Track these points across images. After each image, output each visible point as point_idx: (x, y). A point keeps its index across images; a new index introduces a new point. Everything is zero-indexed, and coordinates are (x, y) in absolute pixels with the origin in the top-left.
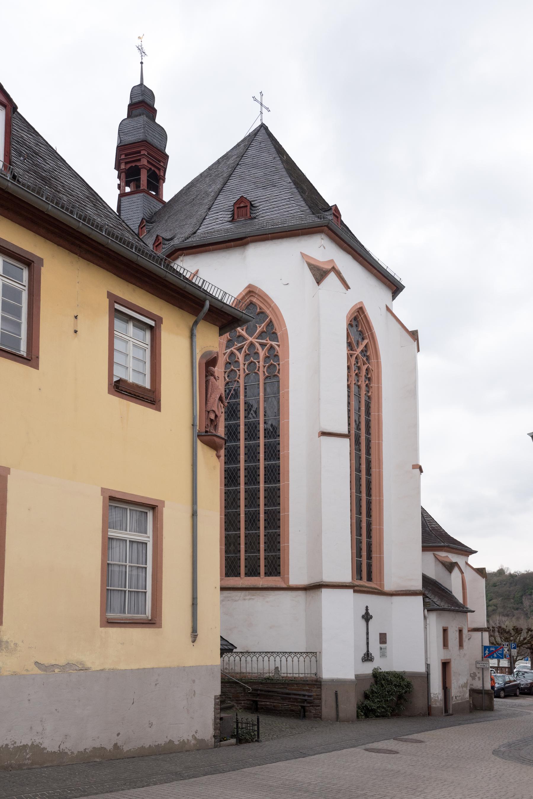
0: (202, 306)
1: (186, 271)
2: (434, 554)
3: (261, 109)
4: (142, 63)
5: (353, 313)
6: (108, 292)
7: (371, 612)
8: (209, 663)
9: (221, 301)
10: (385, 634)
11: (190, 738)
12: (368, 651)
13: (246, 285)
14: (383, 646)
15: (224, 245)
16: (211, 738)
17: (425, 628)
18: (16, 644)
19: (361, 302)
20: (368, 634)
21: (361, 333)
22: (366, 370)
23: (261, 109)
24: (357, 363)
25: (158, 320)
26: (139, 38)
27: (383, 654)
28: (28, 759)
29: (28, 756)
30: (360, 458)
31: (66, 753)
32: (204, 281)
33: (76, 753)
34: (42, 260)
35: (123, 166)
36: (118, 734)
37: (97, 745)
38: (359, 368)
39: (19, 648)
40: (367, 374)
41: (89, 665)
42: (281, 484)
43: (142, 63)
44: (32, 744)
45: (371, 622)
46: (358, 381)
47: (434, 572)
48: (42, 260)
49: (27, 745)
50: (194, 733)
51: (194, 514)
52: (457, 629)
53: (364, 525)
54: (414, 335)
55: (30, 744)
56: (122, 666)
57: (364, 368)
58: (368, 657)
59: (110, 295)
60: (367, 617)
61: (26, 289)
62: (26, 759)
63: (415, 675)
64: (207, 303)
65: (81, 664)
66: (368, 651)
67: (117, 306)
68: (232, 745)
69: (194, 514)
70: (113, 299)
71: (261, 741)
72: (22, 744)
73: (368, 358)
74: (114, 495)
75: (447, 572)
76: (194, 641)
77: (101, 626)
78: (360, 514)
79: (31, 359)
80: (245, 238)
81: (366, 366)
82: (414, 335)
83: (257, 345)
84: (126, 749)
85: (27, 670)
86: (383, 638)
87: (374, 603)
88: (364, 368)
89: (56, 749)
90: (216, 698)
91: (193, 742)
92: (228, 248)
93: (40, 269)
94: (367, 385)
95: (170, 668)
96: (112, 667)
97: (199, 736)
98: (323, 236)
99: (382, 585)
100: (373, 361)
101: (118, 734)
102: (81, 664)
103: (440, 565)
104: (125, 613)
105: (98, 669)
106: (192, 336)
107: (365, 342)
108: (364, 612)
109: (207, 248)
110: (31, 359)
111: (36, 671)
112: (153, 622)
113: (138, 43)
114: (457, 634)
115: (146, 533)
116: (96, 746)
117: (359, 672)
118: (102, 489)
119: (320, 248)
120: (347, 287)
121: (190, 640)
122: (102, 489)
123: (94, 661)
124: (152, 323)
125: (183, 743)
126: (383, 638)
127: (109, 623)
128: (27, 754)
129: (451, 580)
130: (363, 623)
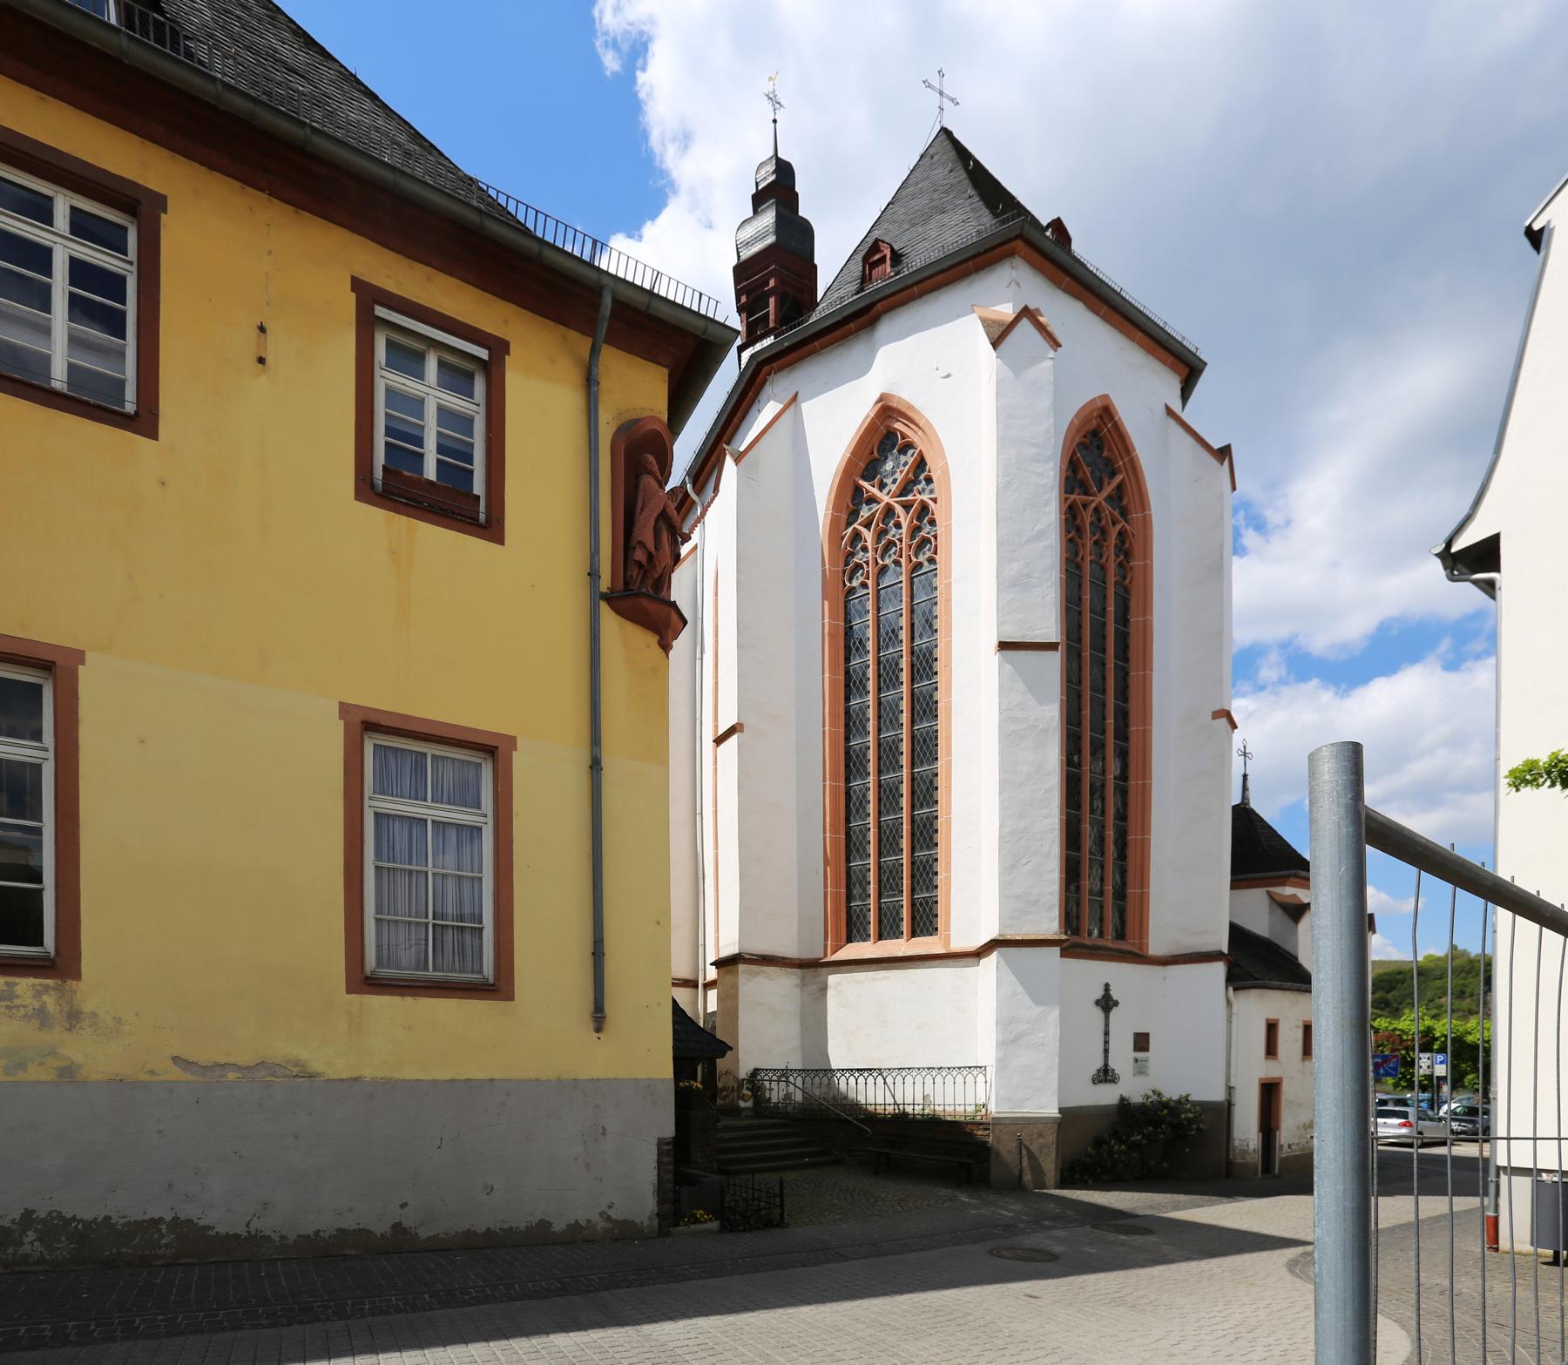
0: (596, 307)
1: (551, 224)
2: (1269, 893)
3: (941, 84)
4: (775, 121)
5: (1087, 420)
6: (354, 279)
7: (1115, 994)
8: (642, 1074)
9: (650, 293)
10: (1146, 1035)
11: (595, 1218)
12: (1106, 1065)
13: (876, 397)
14: (1140, 1055)
15: (838, 333)
16: (650, 1219)
17: (1229, 1021)
18: (118, 1020)
19: (1106, 397)
20: (1107, 1033)
21: (1109, 463)
22: (1120, 533)
23: (941, 84)
24: (1099, 520)
25: (499, 348)
26: (770, 79)
27: (1140, 1069)
28: (166, 1246)
29: (164, 1241)
30: (1080, 697)
31: (268, 1238)
32: (595, 242)
33: (292, 1237)
34: (165, 198)
35: (744, 299)
36: (404, 1205)
37: (349, 1223)
38: (1104, 532)
39: (127, 1028)
40: (1123, 543)
41: (316, 1066)
42: (940, 764)
43: (775, 121)
44: (176, 1218)
45: (1114, 1013)
46: (1101, 556)
47: (1260, 921)
48: (165, 198)
49: (161, 1219)
50: (605, 1208)
51: (595, 766)
52: (1301, 1024)
53: (1110, 834)
54: (1224, 453)
55: (168, 1219)
56: (409, 1074)
57: (1113, 532)
58: (1105, 1075)
59: (358, 285)
60: (1107, 1003)
61: (134, 269)
62: (160, 1247)
63: (1207, 1107)
64: (607, 301)
65: (297, 1065)
66: (1106, 1065)
67: (380, 311)
68: (710, 1232)
69: (595, 766)
70: (367, 296)
71: (787, 1226)
72: (147, 1217)
73: (1124, 513)
74: (374, 718)
75: (1290, 923)
76: (598, 1030)
77: (348, 992)
78: (1078, 807)
79: (144, 421)
80: (873, 305)
81: (1118, 527)
82: (1224, 453)
83: (899, 509)
84: (424, 1233)
85: (152, 1072)
86: (1142, 1042)
87: (1121, 976)
88: (1113, 532)
89: (241, 1230)
90: (661, 1143)
91: (601, 1224)
92: (845, 337)
93: (159, 218)
94: (1120, 565)
95: (537, 1080)
96: (381, 1073)
97: (615, 1214)
98: (1018, 261)
99: (1143, 945)
100: (1135, 515)
101: (404, 1205)
102: (297, 1065)
103: (1279, 912)
104: (426, 969)
105: (345, 1076)
106: (590, 382)
107: (1119, 478)
108: (1099, 994)
109: (810, 346)
110: (144, 421)
111: (176, 1073)
112: (498, 988)
113: (768, 87)
114: (1300, 1033)
115: (479, 807)
116: (346, 1226)
117: (1074, 1101)
118: (342, 705)
119: (1009, 288)
120: (1055, 344)
121: (591, 1026)
122: (342, 705)
123: (330, 1059)
124: (483, 354)
125: (575, 1227)
126: (1142, 1042)
127: (364, 982)
128: (162, 1236)
129: (1296, 934)
130: (1098, 1013)
